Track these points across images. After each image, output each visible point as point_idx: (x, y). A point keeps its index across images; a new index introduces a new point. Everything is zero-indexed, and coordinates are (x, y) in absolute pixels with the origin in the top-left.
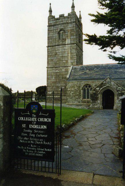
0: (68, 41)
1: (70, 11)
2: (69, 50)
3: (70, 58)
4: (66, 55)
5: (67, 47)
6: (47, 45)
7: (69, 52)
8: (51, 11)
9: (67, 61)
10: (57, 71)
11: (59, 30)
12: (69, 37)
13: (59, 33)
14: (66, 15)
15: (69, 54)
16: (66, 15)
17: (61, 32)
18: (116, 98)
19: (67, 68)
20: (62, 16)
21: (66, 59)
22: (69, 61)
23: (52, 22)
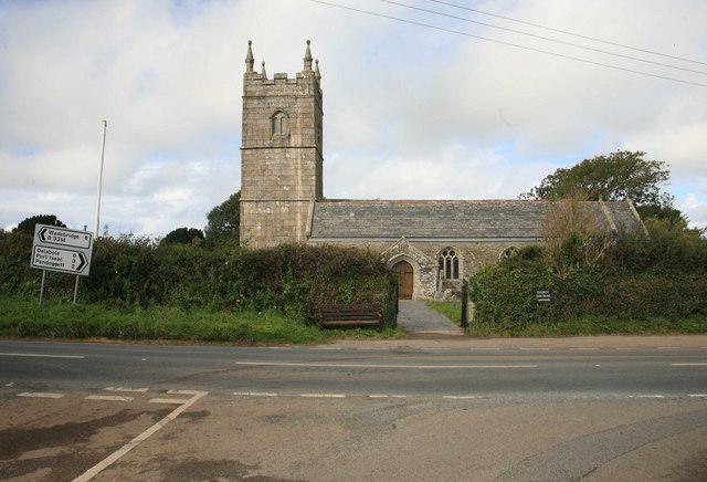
0: (296, 140)
1: (300, 67)
2: (299, 162)
3: (300, 182)
4: (293, 173)
5: (292, 154)
6: (240, 145)
7: (300, 166)
8: (251, 61)
9: (293, 189)
10: (268, 210)
11: (273, 111)
12: (299, 131)
13: (273, 119)
14: (292, 76)
15: (299, 172)
16: (292, 76)
17: (279, 116)
18: (416, 277)
19: (292, 203)
20: (280, 78)
21: (292, 183)
22: (300, 188)
23: (254, 88)
